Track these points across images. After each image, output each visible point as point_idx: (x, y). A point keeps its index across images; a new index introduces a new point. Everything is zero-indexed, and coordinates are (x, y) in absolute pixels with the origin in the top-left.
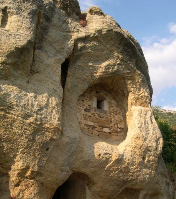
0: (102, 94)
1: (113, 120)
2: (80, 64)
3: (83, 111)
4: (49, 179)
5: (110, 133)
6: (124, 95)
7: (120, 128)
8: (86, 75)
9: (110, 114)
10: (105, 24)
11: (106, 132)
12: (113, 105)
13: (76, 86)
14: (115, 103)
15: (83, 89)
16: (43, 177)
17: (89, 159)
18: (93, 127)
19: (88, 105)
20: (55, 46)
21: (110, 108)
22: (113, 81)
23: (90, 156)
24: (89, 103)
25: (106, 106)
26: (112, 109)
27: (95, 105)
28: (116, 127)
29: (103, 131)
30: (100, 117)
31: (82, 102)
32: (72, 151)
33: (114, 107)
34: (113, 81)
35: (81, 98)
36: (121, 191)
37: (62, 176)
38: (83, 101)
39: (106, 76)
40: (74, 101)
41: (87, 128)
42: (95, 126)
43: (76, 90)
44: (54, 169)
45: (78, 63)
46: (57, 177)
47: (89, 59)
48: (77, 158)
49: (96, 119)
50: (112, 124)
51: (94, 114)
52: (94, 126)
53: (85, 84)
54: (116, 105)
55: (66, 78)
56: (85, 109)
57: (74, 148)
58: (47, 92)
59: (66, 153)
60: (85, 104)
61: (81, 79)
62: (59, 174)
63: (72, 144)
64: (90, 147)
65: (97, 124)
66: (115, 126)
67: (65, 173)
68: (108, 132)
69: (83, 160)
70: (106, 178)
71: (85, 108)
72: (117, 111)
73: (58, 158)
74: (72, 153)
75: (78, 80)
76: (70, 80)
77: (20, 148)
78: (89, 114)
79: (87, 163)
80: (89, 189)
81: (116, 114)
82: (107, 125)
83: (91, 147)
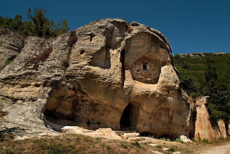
3: (136, 71)
7: (156, 77)
10: (140, 30)
12: (152, 66)
14: (153, 65)
21: (150, 68)
22: (149, 55)
24: (139, 67)
26: (151, 68)
27: (142, 67)
28: (154, 77)
34: (149, 55)
38: (135, 67)
50: (152, 76)
55: (65, 116)
58: (115, 38)
77: (49, 82)
78: (139, 72)
82: (149, 77)
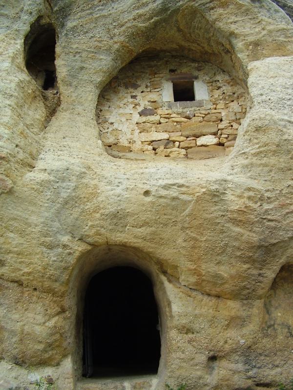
0: (185, 70)
1: (223, 114)
2: (74, 24)
4: (26, 270)
5: (220, 144)
6: (228, 52)
8: (95, 39)
9: (214, 104)
11: (208, 146)
13: (82, 68)
14: (227, 78)
15: (100, 70)
16: (7, 268)
17: (119, 208)
18: (169, 142)
19: (149, 102)
20: (6, 12)
23: (120, 201)
24: (153, 96)
25: (201, 91)
29: (198, 144)
30: (189, 118)
31: (131, 100)
32: (61, 199)
33: (224, 88)
35: (127, 93)
36: (270, 274)
37: (55, 259)
39: (148, 24)
40: (86, 100)
41: (150, 147)
42: (173, 139)
43: (85, 77)
44: (24, 246)
45: (70, 24)
46: (42, 262)
47: (90, 6)
48: (83, 212)
49: (175, 124)
51: (168, 114)
52: (170, 139)
53: (101, 57)
54: (229, 83)
56: (142, 111)
57: (69, 191)
59: (46, 205)
60: (140, 102)
61: (87, 51)
62: (46, 255)
63: (58, 185)
64: (117, 181)
65: (180, 133)
66: (232, 126)
67: (60, 250)
68: (212, 143)
69: (102, 215)
70: (194, 247)
71: (140, 109)
72: (234, 94)
73: (27, 219)
74: (66, 203)
75: (81, 56)
76: (63, 62)
79: (118, 218)
80: (170, 281)
81: (233, 101)
83: (120, 180)
